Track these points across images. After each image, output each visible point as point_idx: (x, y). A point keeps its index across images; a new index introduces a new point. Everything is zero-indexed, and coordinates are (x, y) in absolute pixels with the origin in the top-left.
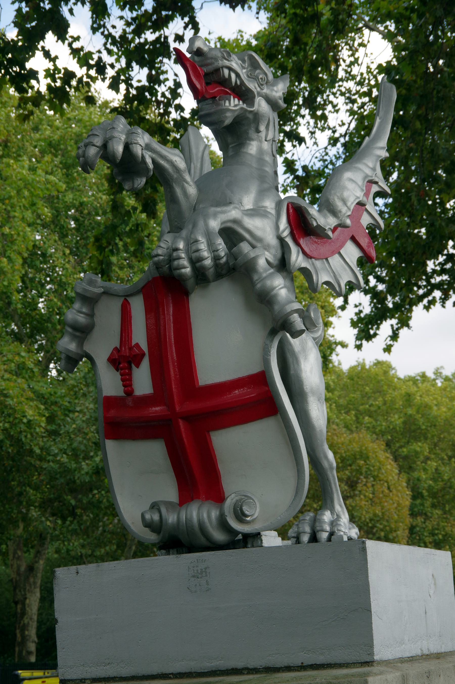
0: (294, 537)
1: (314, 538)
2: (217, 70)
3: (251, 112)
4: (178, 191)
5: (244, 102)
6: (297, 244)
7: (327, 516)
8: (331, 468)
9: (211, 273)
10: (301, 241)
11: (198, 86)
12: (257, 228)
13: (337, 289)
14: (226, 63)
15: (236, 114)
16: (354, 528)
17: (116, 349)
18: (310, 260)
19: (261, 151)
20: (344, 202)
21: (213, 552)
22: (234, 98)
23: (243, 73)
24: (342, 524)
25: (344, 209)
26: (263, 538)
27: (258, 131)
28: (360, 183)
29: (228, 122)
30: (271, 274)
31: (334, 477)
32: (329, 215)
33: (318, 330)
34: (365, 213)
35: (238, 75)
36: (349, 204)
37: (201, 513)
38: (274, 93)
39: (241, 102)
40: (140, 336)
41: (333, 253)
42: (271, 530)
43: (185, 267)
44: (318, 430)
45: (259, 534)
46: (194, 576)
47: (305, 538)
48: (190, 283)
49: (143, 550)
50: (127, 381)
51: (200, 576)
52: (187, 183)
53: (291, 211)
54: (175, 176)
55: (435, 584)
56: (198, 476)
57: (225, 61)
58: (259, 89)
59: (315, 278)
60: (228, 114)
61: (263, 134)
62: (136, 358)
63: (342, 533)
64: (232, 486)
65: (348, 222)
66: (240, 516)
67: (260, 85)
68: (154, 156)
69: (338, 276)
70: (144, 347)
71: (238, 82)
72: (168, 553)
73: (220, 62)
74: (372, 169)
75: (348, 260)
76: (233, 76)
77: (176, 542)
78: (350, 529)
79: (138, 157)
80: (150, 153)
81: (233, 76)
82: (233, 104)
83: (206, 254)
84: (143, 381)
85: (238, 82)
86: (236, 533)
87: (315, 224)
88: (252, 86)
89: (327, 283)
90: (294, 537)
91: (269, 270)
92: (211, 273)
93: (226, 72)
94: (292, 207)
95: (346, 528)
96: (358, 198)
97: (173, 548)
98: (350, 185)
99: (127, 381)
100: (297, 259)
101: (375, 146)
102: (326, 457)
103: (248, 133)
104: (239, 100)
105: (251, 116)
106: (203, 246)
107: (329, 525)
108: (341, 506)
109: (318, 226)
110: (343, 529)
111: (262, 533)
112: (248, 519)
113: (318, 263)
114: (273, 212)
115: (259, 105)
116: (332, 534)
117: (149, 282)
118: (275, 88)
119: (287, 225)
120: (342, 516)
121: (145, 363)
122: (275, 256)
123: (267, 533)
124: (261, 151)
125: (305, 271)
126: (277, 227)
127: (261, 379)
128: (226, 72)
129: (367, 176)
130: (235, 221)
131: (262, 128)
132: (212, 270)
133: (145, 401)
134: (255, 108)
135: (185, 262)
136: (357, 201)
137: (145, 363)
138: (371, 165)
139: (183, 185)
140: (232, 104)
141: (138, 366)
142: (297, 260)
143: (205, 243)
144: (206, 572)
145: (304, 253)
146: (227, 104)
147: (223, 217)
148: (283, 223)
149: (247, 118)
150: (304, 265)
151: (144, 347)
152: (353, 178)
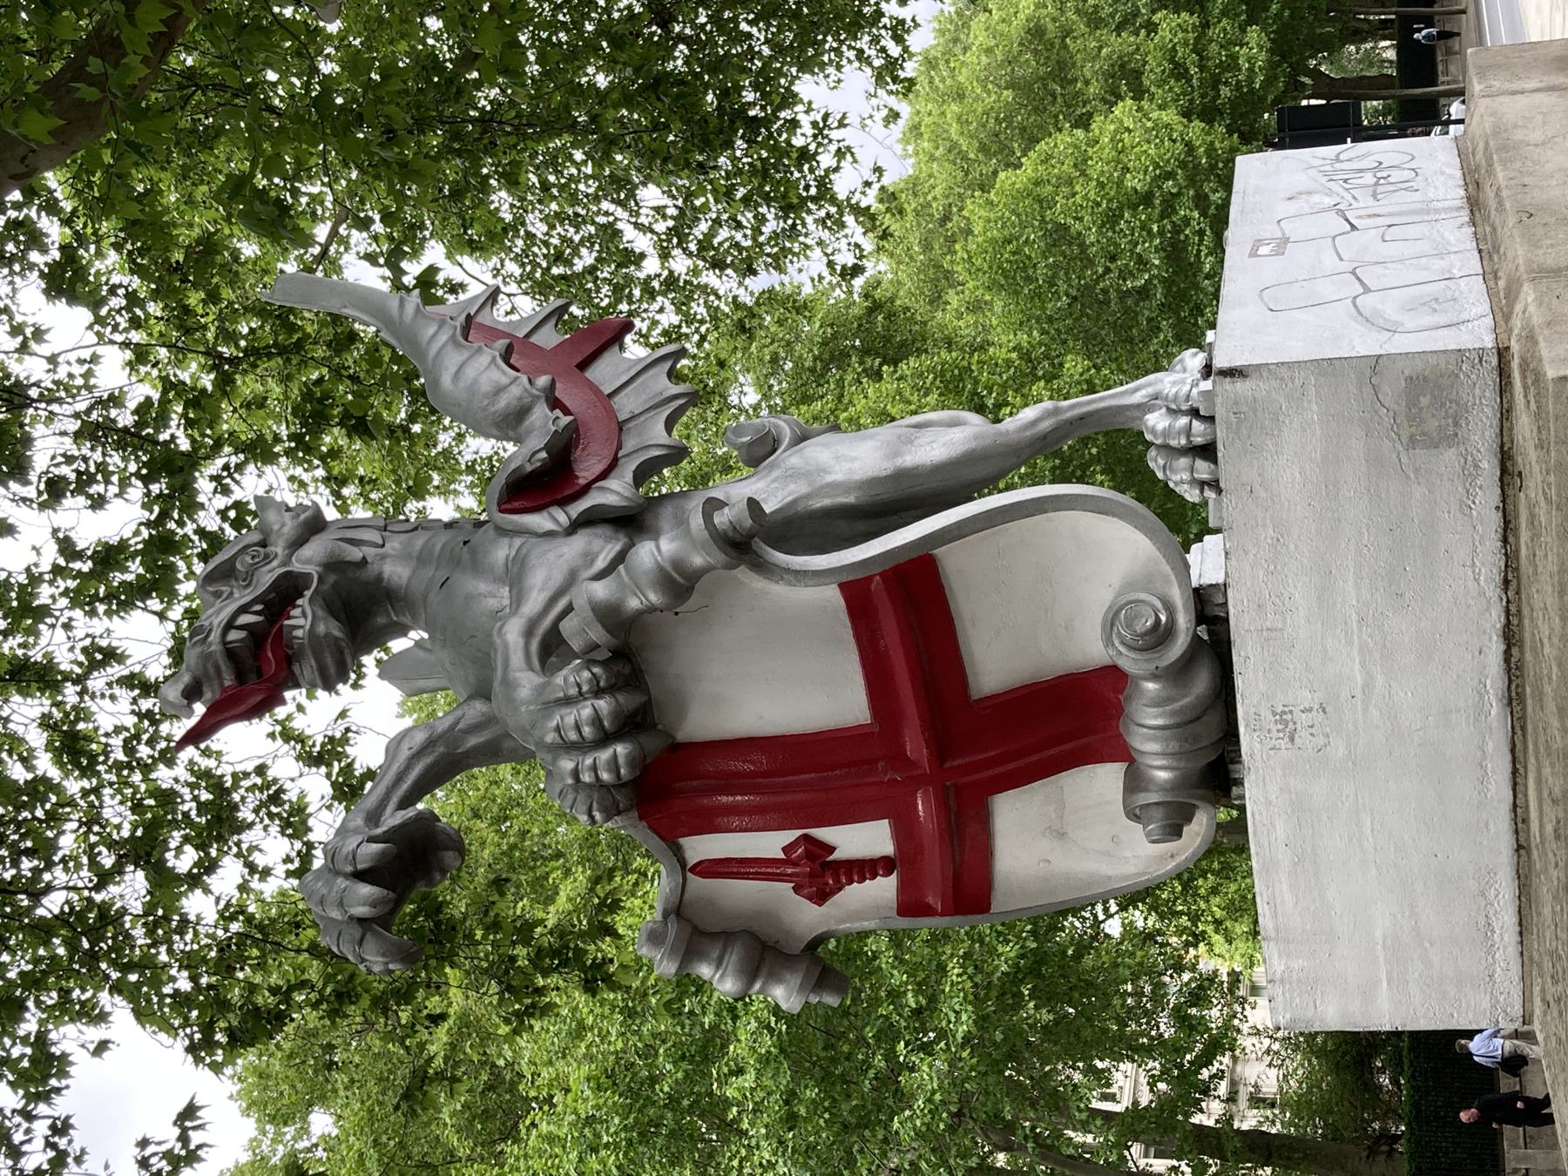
0: (1202, 492)
1: (1207, 451)
2: (230, 653)
3: (320, 579)
4: (473, 741)
5: (301, 595)
6: (585, 490)
7: (1156, 421)
8: (1056, 411)
9: (628, 700)
10: (582, 482)
11: (258, 698)
12: (545, 583)
13: (681, 401)
14: (215, 637)
15: (320, 613)
16: (1181, 361)
17: (796, 890)
18: (621, 462)
19: (404, 556)
20: (499, 390)
21: (1238, 696)
22: (289, 618)
23: (243, 597)
24: (1174, 390)
25: (515, 391)
26: (1206, 581)
27: (364, 561)
28: (466, 354)
29: (336, 631)
30: (627, 569)
31: (1073, 407)
32: (526, 423)
33: (777, 426)
34: (533, 339)
35: (244, 609)
36: (505, 380)
37: (1150, 722)
38: (286, 530)
39: (299, 602)
40: (770, 844)
41: (611, 412)
42: (1187, 567)
43: (615, 755)
44: (973, 445)
45: (1196, 591)
46: (1292, 740)
47: (1203, 469)
48: (653, 744)
49: (1231, 842)
50: (865, 869)
51: (1291, 725)
52: (457, 722)
53: (516, 505)
54: (442, 749)
55: (1309, 193)
56: (1068, 720)
57: (211, 638)
58: (275, 563)
59: (657, 452)
60: (321, 629)
61: (370, 552)
62: (818, 851)
63: (1195, 391)
64: (1089, 647)
65: (543, 381)
66: (1160, 635)
67: (268, 559)
68: (395, 800)
69: (657, 400)
70: (790, 836)
71: (258, 607)
72: (1239, 783)
73: (213, 648)
74: (440, 327)
75: (625, 379)
76: (245, 619)
77: (1216, 772)
78: (1185, 370)
79: (383, 853)
80: (389, 809)
81: (245, 619)
82: (302, 619)
83: (586, 712)
84: (867, 838)
85: (258, 607)
86: (1196, 639)
87: (544, 455)
88: (266, 578)
89: (669, 425)
90: (1202, 492)
91: (619, 575)
92: (628, 700)
93: (234, 635)
94: (508, 502)
95: (1183, 382)
96: (494, 359)
97: (1227, 772)
98: (470, 373)
99: (865, 869)
100: (616, 492)
101: (397, 318)
102: (1034, 423)
103: (368, 583)
104: (294, 607)
105: (332, 578)
106: (569, 717)
107: (1176, 419)
108: (1136, 390)
109: (546, 448)
110: (1186, 388)
111: (1195, 584)
112: (1163, 618)
113: (630, 444)
114: (518, 542)
115: (308, 562)
116: (1195, 413)
117: (650, 827)
118: (276, 527)
119: (545, 514)
120: (1158, 387)
121: (824, 834)
122: (608, 540)
123: (1194, 573)
124: (404, 556)
125: (642, 475)
126: (550, 534)
127: (858, 593)
128: (234, 635)
129: (453, 338)
130: (529, 633)
131: (355, 554)
132: (621, 698)
133: (904, 832)
134: (312, 569)
135: (604, 755)
136: (500, 361)
137: (824, 834)
138: (431, 330)
139: (461, 731)
140: (301, 622)
141: (832, 849)
142: (618, 493)
143: (564, 711)
144: (1284, 713)
145: (604, 475)
146: (299, 633)
147: (517, 659)
148: (537, 521)
149: (335, 584)
150: (629, 477)
151: (790, 836)
152: (452, 370)
